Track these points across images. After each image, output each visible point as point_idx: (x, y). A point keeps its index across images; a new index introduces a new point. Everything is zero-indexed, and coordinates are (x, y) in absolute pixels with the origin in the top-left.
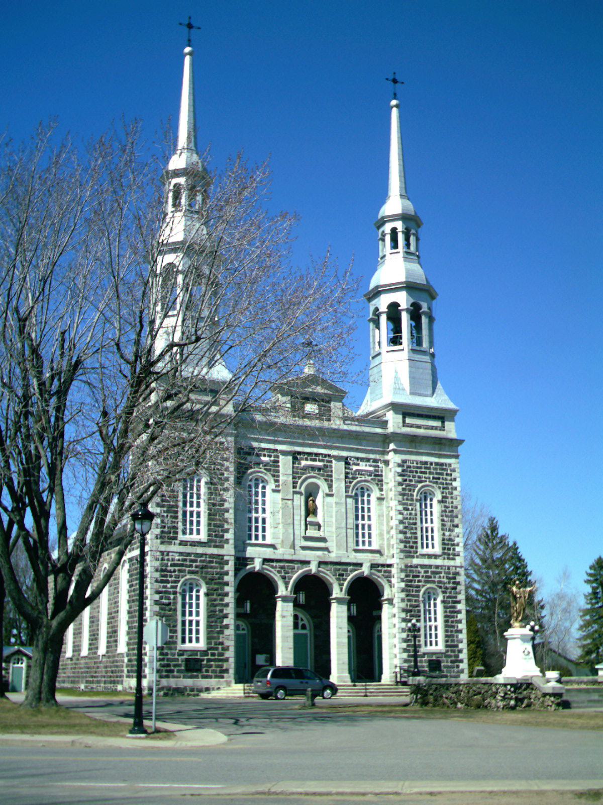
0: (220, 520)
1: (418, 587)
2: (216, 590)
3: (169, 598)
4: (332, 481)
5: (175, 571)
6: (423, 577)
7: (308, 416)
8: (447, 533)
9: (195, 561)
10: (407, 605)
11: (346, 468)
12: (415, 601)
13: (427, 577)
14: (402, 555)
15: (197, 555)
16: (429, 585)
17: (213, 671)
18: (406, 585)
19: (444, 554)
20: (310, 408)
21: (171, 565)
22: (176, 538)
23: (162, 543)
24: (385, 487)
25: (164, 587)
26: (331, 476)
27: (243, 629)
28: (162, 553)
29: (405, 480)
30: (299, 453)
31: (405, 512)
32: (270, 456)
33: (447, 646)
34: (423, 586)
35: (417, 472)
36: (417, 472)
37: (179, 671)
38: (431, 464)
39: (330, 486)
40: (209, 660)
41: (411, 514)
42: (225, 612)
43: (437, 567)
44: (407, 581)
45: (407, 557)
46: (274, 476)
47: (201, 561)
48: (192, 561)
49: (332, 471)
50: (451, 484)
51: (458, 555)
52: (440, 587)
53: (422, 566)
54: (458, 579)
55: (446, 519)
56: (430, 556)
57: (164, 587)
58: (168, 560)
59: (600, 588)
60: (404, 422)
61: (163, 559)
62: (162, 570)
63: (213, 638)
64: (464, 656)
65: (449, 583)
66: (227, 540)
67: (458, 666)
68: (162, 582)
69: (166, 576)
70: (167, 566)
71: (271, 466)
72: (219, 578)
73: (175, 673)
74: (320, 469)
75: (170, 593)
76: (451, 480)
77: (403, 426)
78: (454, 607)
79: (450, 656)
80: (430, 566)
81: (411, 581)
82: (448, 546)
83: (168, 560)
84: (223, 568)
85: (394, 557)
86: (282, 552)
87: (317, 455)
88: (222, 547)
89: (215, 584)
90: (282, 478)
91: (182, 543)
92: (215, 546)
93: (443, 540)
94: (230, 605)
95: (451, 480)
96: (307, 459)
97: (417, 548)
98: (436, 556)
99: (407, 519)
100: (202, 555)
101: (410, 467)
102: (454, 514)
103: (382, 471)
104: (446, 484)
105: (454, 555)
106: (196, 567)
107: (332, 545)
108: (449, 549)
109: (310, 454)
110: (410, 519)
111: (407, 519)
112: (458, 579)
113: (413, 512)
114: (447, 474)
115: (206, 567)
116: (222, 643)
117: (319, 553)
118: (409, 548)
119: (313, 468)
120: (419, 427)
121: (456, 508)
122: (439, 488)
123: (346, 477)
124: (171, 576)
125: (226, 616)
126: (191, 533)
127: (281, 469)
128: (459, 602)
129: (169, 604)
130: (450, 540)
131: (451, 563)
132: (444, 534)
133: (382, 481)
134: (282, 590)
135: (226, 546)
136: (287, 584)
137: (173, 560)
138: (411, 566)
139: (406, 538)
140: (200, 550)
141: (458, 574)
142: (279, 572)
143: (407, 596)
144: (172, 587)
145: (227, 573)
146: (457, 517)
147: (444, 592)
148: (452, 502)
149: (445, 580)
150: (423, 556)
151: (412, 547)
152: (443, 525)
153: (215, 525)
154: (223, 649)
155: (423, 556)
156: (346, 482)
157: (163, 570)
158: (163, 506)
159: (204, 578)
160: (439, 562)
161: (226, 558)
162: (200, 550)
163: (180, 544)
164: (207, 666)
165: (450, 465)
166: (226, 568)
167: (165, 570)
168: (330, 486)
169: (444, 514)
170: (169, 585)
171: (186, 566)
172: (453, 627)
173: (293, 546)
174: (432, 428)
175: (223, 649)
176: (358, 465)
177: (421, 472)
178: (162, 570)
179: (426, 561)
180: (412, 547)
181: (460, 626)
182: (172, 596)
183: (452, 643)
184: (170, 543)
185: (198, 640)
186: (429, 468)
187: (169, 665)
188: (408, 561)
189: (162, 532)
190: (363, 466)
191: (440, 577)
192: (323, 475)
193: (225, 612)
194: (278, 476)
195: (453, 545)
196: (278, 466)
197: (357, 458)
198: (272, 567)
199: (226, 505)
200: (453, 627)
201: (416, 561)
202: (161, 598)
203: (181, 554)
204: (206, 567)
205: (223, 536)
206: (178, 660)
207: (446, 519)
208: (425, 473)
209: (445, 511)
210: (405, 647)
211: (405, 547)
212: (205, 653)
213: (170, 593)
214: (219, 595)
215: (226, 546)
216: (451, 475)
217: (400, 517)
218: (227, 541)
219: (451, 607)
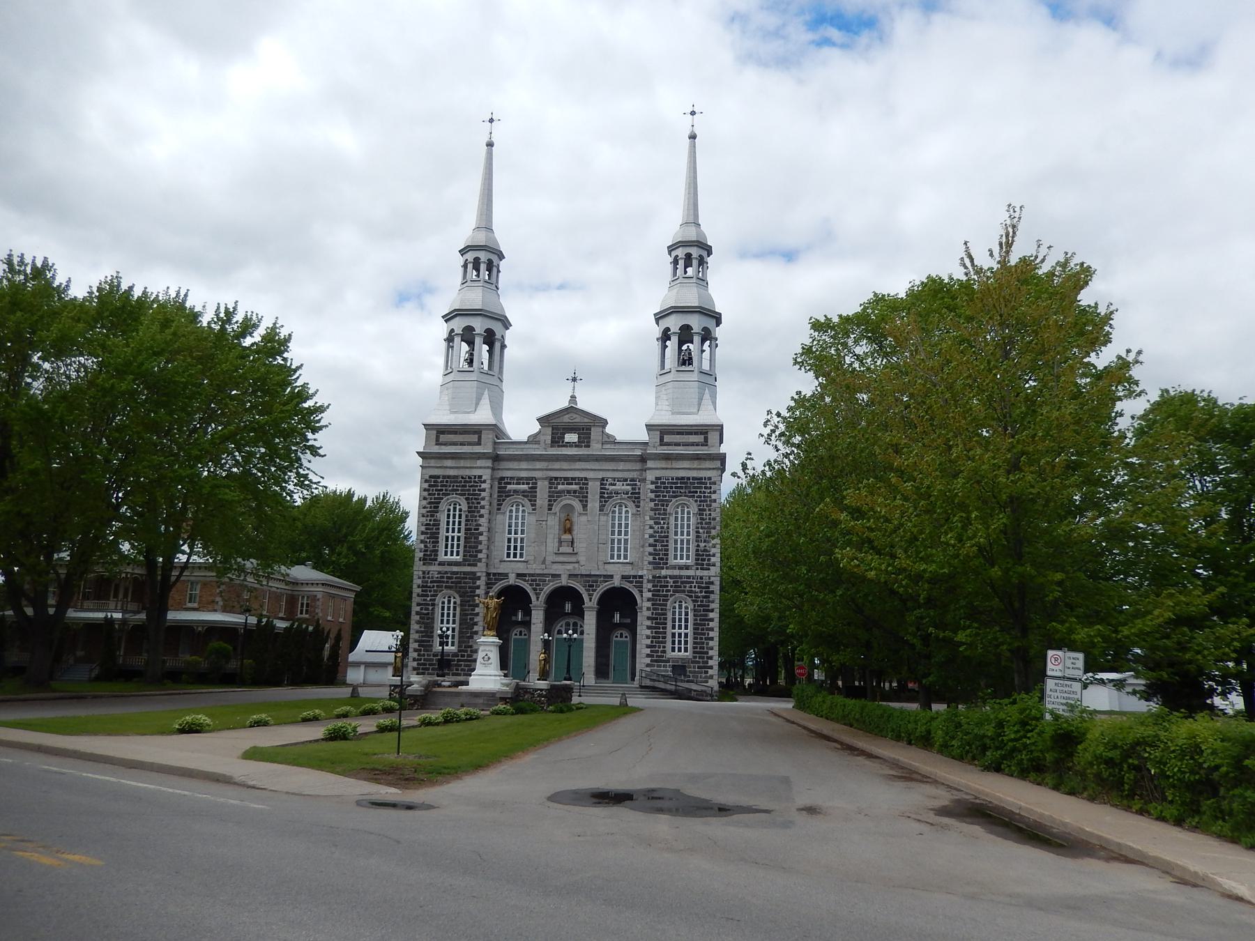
0: (475, 542)
1: (667, 596)
2: (469, 601)
3: (427, 609)
4: (587, 501)
5: (433, 587)
6: (671, 586)
7: (570, 445)
8: (702, 545)
9: (451, 578)
10: (653, 613)
11: (601, 488)
12: (662, 610)
13: (676, 587)
14: (651, 567)
15: (453, 573)
16: (677, 595)
17: (462, 670)
18: (653, 595)
19: (697, 564)
20: (571, 437)
21: (431, 582)
22: (436, 560)
23: (424, 564)
24: (642, 503)
25: (424, 600)
26: (587, 497)
27: (626, 637)
28: (424, 573)
29: (659, 496)
30: (556, 478)
31: (656, 527)
32: (528, 484)
33: (694, 652)
34: (671, 596)
35: (671, 488)
36: (671, 488)
37: (433, 669)
38: (689, 478)
39: (585, 507)
40: (459, 661)
41: (662, 528)
42: (475, 620)
43: (689, 577)
44: (654, 591)
45: (654, 568)
46: (530, 501)
47: (456, 578)
48: (448, 578)
49: (587, 493)
50: (710, 497)
51: (714, 565)
52: (691, 597)
53: (671, 577)
54: (712, 588)
55: (701, 531)
56: (681, 568)
57: (424, 600)
58: (429, 578)
59: (54, 609)
60: (662, 439)
61: (424, 577)
62: (423, 586)
63: (464, 642)
64: (714, 662)
65: (701, 592)
66: (481, 559)
67: (707, 672)
68: (422, 596)
69: (426, 591)
70: (427, 582)
71: (529, 492)
72: (471, 592)
73: (430, 671)
74: (575, 492)
75: (428, 605)
76: (710, 493)
77: (661, 445)
78: (706, 615)
79: (699, 662)
80: (681, 577)
81: (659, 591)
82: (702, 559)
83: (429, 578)
84: (475, 583)
85: (646, 572)
86: (535, 568)
87: (573, 479)
88: (476, 565)
89: (468, 596)
90: (539, 502)
91: (441, 564)
92: (469, 565)
93: (697, 550)
94: (715, 610)
95: (710, 493)
96: (563, 484)
97: (667, 559)
98: (687, 567)
99: (658, 532)
100: (457, 573)
101: (664, 483)
102: (712, 526)
103: (639, 489)
104: (704, 497)
105: (709, 565)
106: (452, 583)
107: (582, 559)
108: (704, 560)
109: (566, 479)
110: (661, 532)
111: (658, 532)
112: (712, 588)
113: (665, 526)
114: (706, 488)
115: (460, 583)
116: (471, 647)
117: (570, 567)
118: (660, 560)
119: (569, 492)
120: (677, 444)
121: (714, 519)
122: (696, 501)
123: (601, 497)
124: (430, 591)
125: (476, 624)
126: (452, 555)
127: (538, 494)
128: (712, 611)
129: (428, 614)
130: (705, 550)
131: (705, 573)
132: (698, 546)
133: (639, 498)
134: (587, 603)
135: (479, 564)
136: (538, 595)
137: (432, 578)
138: (659, 577)
139: (655, 550)
140: (455, 569)
141: (712, 583)
142: (531, 585)
143: (653, 605)
144: (431, 600)
145: (478, 587)
146: (714, 528)
147: (694, 601)
148: (710, 515)
149: (697, 590)
150: (674, 567)
151: (662, 559)
152: (698, 537)
153: (470, 547)
154: (472, 651)
155: (674, 567)
156: (601, 502)
157: (424, 586)
158: (426, 533)
159: (458, 592)
160: (690, 573)
161: (478, 574)
162: (455, 569)
163: (439, 565)
164: (456, 665)
165: (710, 478)
166: (478, 583)
167: (426, 586)
168: (585, 507)
169: (700, 526)
170: (428, 599)
171: (443, 582)
172: (704, 634)
173: (544, 562)
174: (693, 444)
175: (472, 651)
176: (615, 485)
177: (676, 488)
178: (423, 586)
179: (676, 572)
180: (662, 559)
181: (711, 634)
182: (430, 608)
183: (701, 652)
184: (431, 564)
185: (686, 650)
186: (686, 483)
187: (425, 664)
188: (657, 573)
189: (424, 555)
190: (619, 486)
191: (691, 587)
192: (577, 497)
193: (475, 620)
194: (535, 501)
195: (709, 555)
196: (536, 492)
197: (614, 479)
198: (525, 580)
199: (481, 529)
200: (704, 634)
201: (664, 572)
202: (421, 609)
203: (439, 573)
204: (460, 583)
205: (476, 556)
206: (433, 660)
207: (701, 531)
208: (681, 488)
209: (701, 523)
210: (649, 652)
211: (654, 559)
212: (455, 655)
213: (428, 605)
214: (470, 606)
215: (479, 564)
216: (711, 488)
217: (651, 531)
218: (480, 560)
219: (701, 615)
